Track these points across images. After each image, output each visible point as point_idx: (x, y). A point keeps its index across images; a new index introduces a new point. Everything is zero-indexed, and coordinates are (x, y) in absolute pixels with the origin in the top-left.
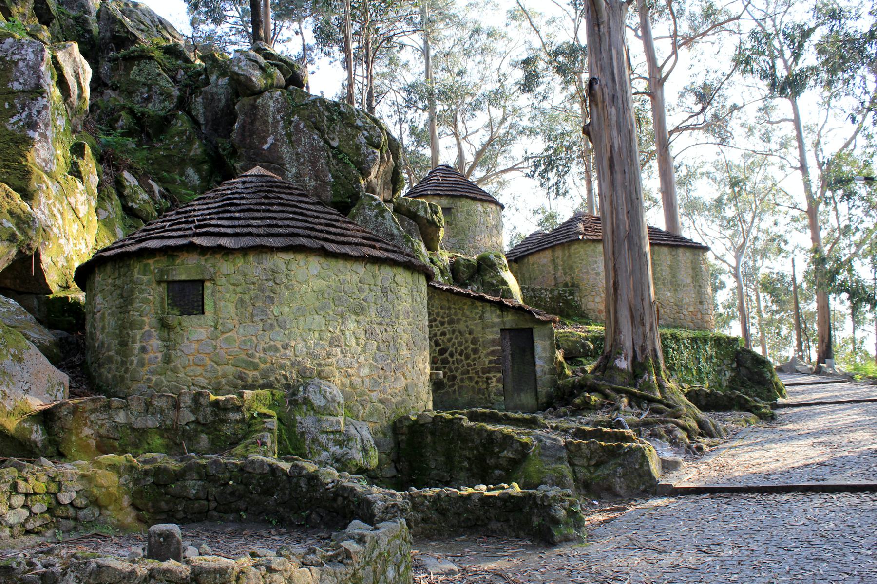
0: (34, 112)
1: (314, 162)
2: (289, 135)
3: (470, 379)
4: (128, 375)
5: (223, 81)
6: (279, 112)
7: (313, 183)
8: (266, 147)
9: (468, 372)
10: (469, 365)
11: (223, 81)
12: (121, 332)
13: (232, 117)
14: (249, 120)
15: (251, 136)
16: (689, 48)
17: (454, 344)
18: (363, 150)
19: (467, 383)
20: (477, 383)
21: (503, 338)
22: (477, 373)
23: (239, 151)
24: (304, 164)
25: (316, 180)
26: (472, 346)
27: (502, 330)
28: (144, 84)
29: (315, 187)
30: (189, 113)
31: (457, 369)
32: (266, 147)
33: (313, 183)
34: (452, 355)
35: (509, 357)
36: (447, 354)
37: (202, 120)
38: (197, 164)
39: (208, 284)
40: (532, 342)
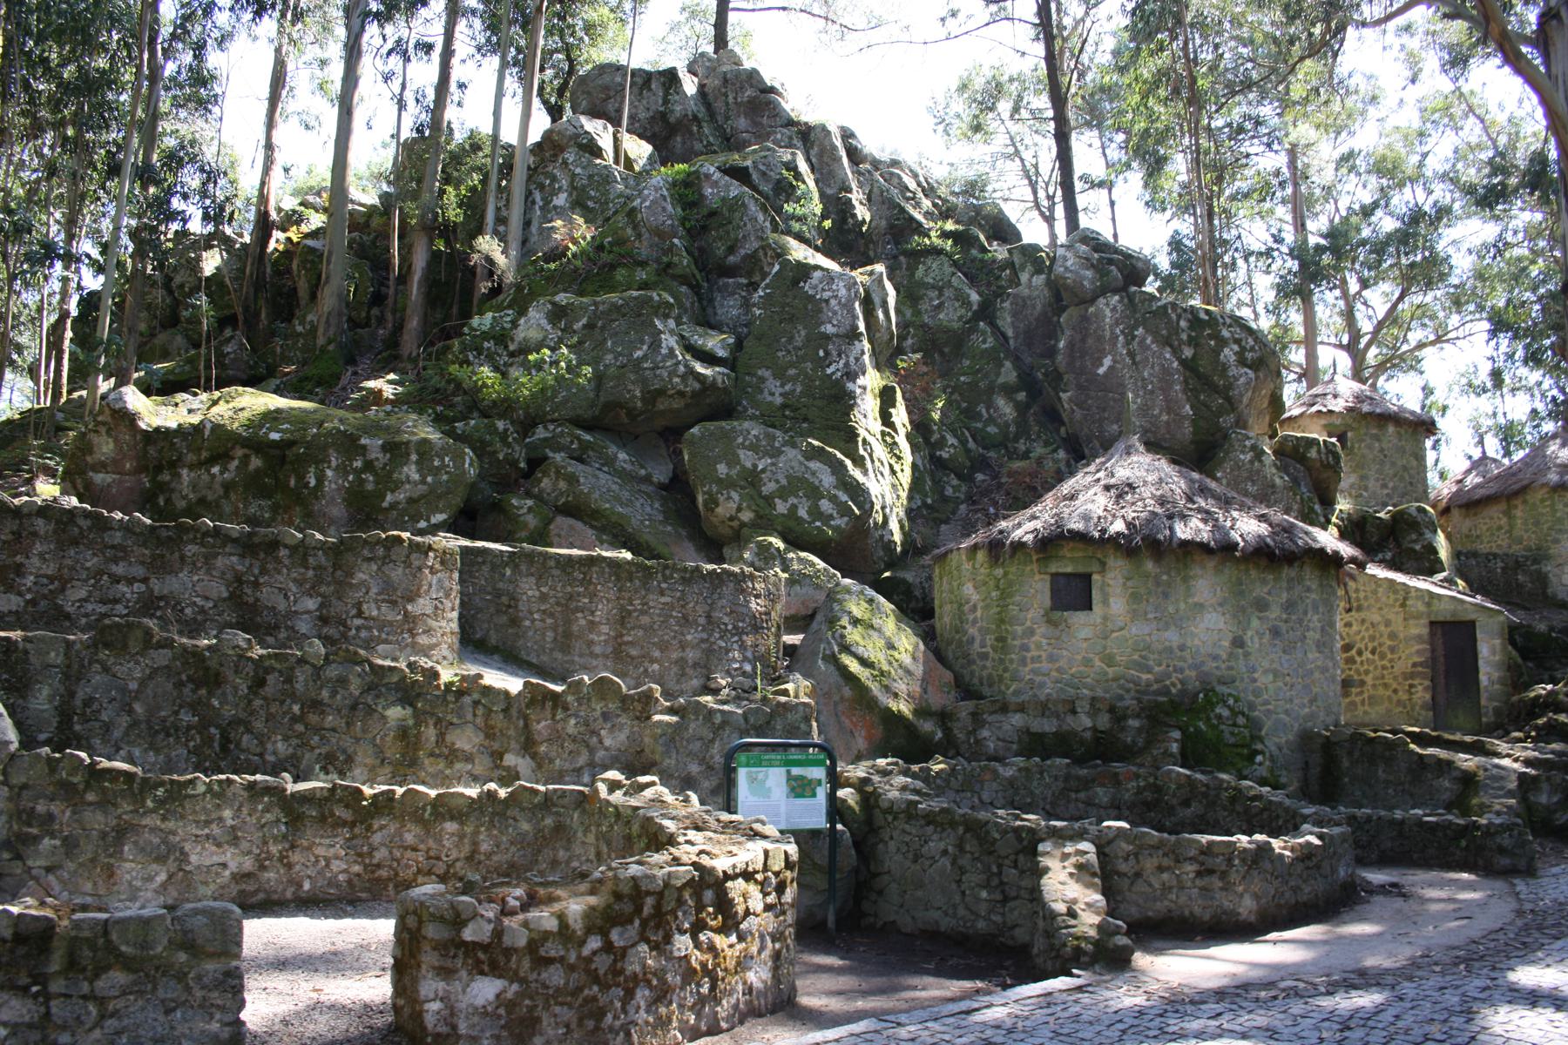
0: (852, 359)
1: (1166, 387)
2: (1131, 354)
3: (1386, 686)
4: (1006, 675)
5: (1039, 280)
6: (1117, 324)
7: (1165, 418)
8: (1101, 371)
9: (1383, 677)
10: (1384, 668)
11: (1039, 280)
12: (998, 626)
13: (1053, 332)
14: (1078, 337)
15: (1082, 357)
16: (1539, 555)
17: (1363, 639)
18: (1233, 371)
19: (1381, 691)
20: (1395, 691)
21: (1432, 634)
22: (1395, 678)
23: (1066, 377)
24: (1152, 392)
25: (1168, 413)
26: (1389, 643)
27: (1432, 623)
28: (933, 287)
29: (1167, 423)
30: (992, 324)
31: (1367, 672)
32: (1101, 371)
33: (1165, 418)
34: (1360, 653)
35: (1442, 659)
36: (1354, 652)
37: (1010, 333)
38: (1009, 391)
39: (1095, 577)
40: (1475, 640)
